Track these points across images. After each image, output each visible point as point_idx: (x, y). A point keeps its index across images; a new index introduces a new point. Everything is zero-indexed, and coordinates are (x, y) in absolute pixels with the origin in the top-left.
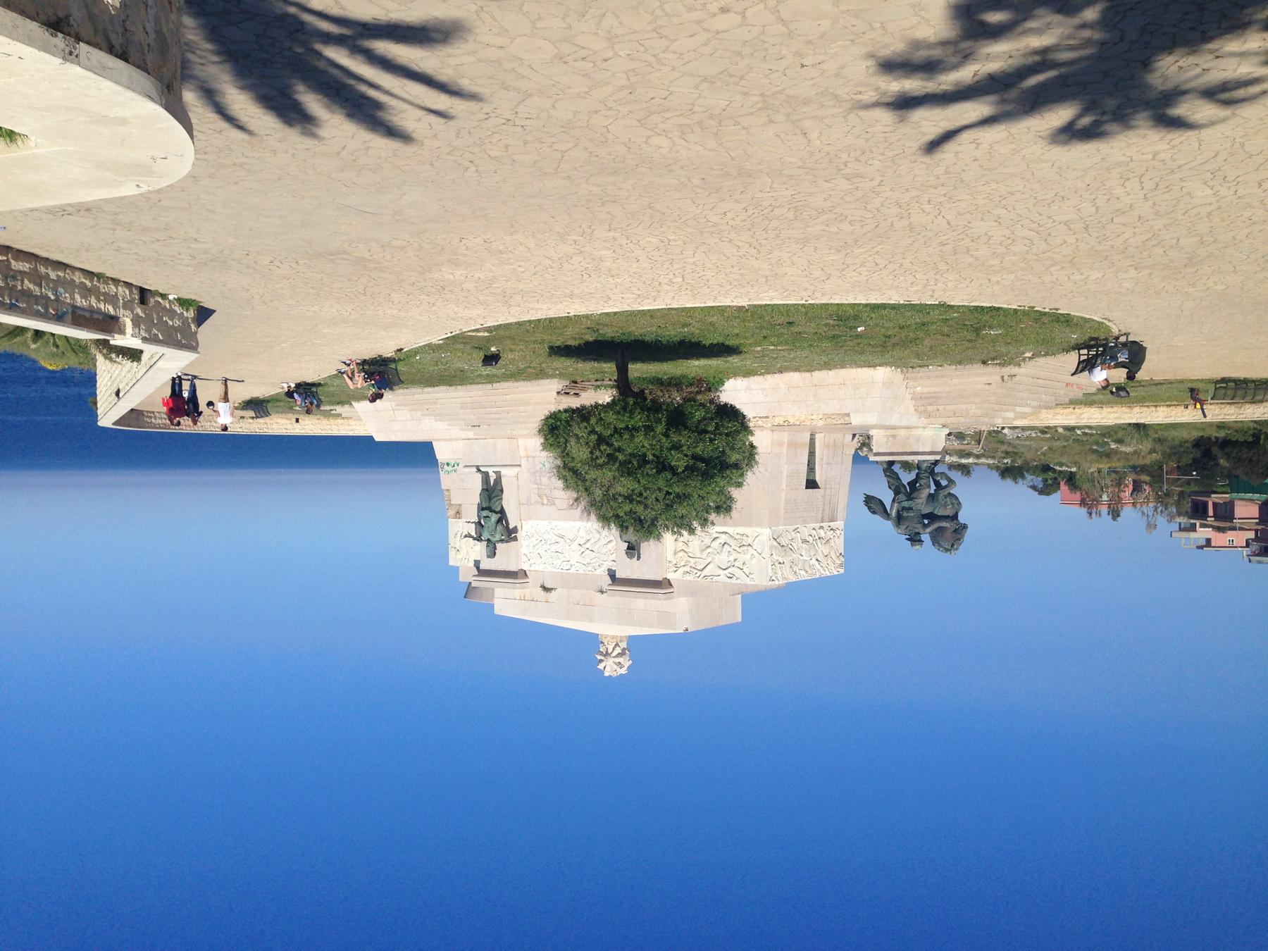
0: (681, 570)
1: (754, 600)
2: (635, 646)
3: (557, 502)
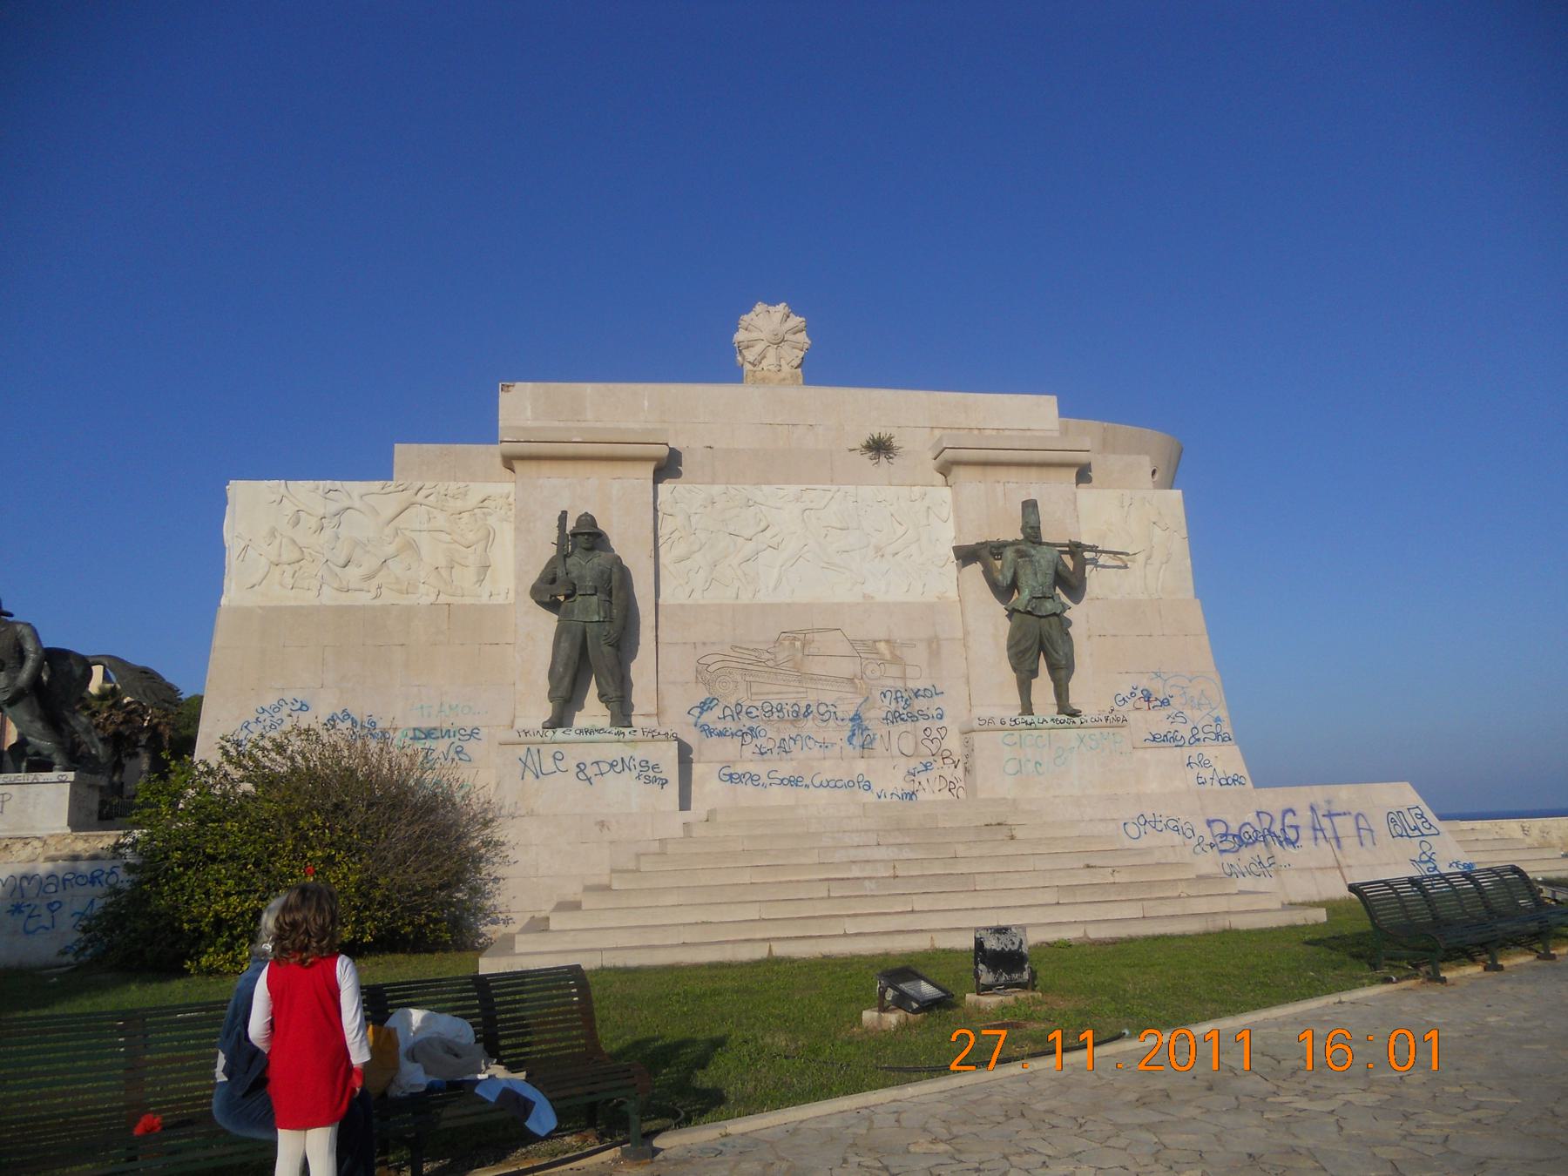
0: (473, 500)
1: (381, 469)
2: (718, 363)
3: (845, 648)
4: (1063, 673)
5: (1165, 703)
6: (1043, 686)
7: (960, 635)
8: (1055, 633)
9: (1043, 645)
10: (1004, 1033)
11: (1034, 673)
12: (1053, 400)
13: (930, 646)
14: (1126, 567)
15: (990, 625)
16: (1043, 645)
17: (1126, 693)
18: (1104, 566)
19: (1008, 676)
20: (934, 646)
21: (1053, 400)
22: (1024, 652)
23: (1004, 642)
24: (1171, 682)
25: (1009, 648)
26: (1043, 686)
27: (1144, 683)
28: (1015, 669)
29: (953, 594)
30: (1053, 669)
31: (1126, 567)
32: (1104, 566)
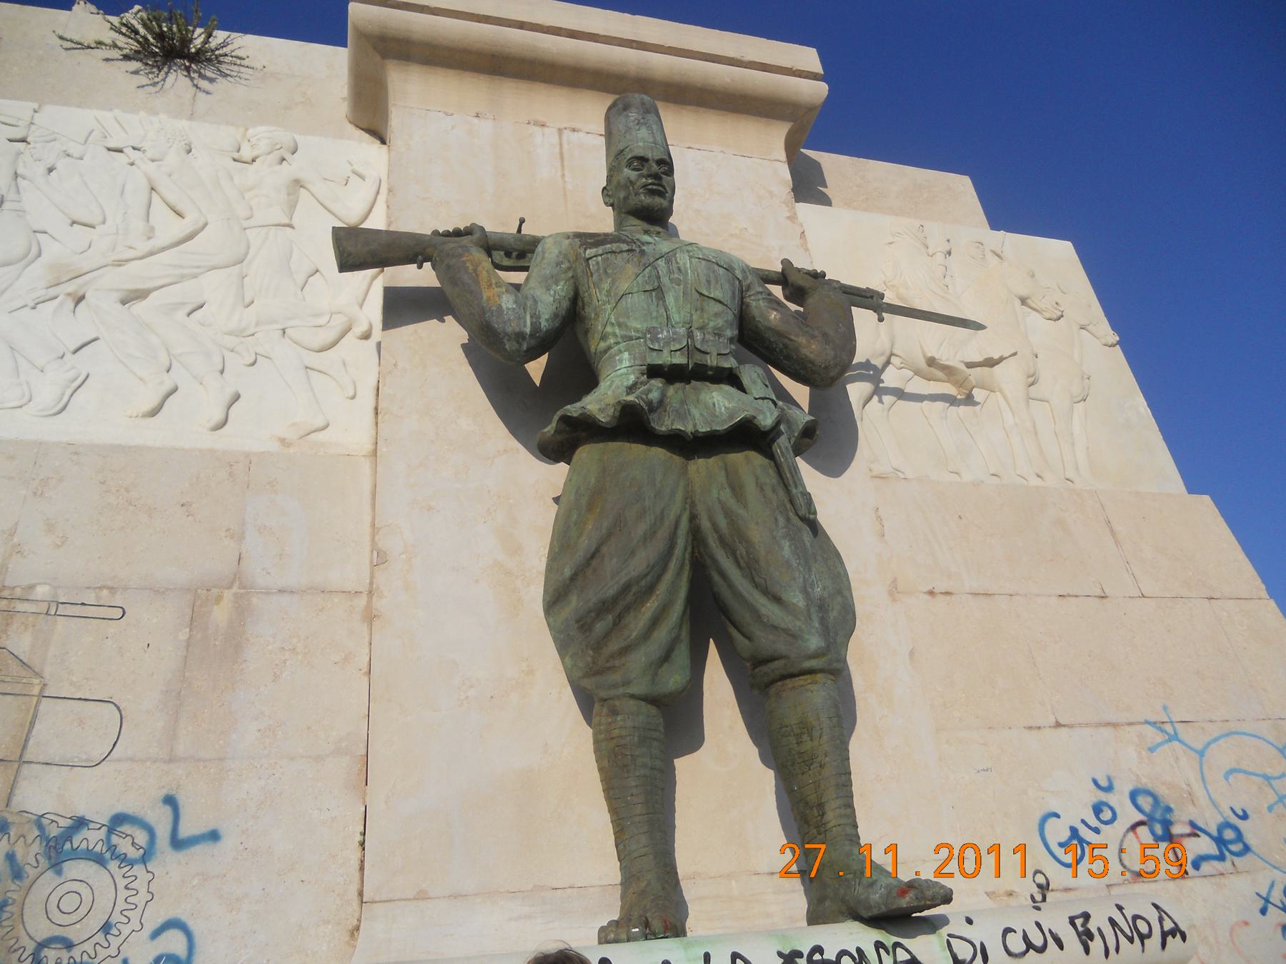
4: (815, 696)
5: (1229, 843)
6: (725, 788)
7: (353, 573)
8: (762, 527)
9: (710, 614)
10: (823, 847)
11: (678, 722)
12: (676, 761)
13: (195, 619)
14: (969, 400)
15: (500, 505)
16: (710, 614)
17: (1076, 811)
18: (900, 394)
19: (557, 740)
20: (217, 623)
21: (676, 761)
22: (616, 607)
23: (535, 594)
24: (1222, 757)
25: (553, 601)
26: (725, 788)
27: (1132, 764)
28: (587, 701)
29: (352, 431)
30: (760, 683)
31: (969, 400)
32: (900, 394)
